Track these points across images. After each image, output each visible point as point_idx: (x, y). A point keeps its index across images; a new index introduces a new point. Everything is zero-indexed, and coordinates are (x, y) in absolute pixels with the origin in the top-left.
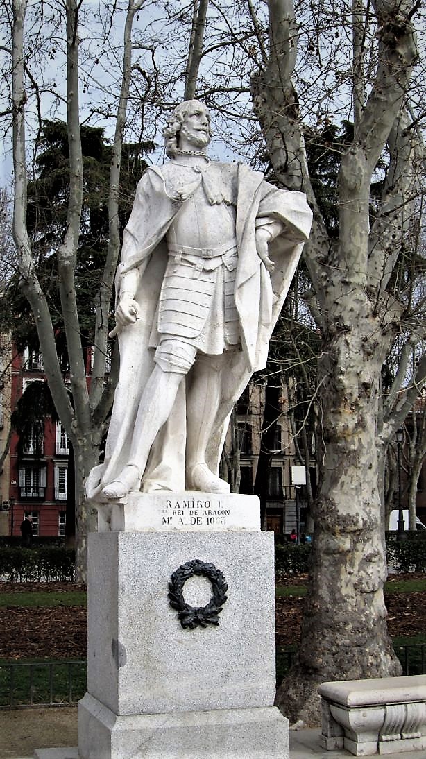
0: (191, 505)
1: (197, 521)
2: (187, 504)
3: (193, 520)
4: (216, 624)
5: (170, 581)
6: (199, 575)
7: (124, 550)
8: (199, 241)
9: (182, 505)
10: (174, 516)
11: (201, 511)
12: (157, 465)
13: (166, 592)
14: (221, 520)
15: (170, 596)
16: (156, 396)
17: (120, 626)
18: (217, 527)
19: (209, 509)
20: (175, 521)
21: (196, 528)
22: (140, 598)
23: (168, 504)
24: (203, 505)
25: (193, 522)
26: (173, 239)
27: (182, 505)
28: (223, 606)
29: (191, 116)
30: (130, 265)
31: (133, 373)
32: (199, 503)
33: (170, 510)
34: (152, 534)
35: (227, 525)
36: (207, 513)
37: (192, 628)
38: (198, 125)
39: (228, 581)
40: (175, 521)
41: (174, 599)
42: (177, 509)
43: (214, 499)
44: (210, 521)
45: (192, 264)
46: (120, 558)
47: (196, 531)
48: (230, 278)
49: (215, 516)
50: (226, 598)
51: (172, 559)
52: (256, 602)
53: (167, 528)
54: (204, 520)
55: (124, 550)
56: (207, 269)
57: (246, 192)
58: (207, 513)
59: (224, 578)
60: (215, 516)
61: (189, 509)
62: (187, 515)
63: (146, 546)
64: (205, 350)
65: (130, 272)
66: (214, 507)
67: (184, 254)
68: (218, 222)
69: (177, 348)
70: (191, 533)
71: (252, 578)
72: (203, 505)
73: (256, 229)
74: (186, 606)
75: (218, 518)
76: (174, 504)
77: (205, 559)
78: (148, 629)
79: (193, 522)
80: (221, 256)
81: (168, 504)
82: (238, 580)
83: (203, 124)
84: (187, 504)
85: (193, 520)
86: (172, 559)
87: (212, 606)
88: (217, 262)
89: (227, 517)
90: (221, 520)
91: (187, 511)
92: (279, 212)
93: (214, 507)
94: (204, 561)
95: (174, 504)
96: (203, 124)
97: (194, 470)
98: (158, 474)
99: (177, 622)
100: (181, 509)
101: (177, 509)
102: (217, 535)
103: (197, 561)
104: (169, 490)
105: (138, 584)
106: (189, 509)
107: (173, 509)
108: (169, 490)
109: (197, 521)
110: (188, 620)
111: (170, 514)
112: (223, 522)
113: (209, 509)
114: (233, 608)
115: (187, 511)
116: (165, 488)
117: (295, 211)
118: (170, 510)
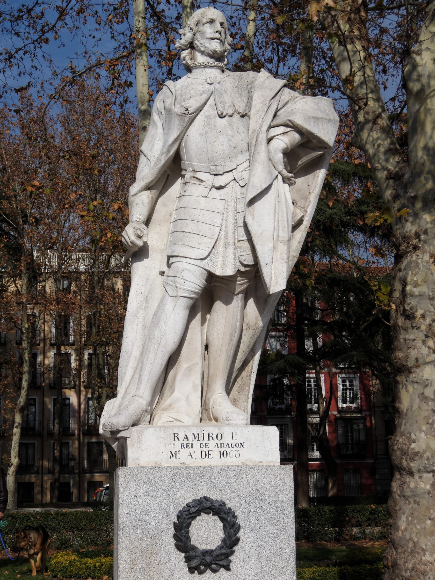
0: (201, 438)
1: (208, 455)
2: (196, 437)
3: (204, 453)
4: (228, 568)
5: (176, 520)
6: (208, 513)
7: (125, 486)
8: (208, 156)
9: (191, 437)
10: (182, 450)
11: (212, 444)
12: (171, 395)
13: (172, 531)
14: (235, 453)
15: (175, 536)
16: (162, 322)
17: (120, 570)
18: (229, 461)
19: (221, 441)
20: (184, 455)
21: (206, 462)
22: (142, 539)
23: (176, 437)
24: (214, 436)
25: (204, 456)
26: (184, 155)
27: (191, 437)
28: (235, 548)
29: (204, 24)
30: (140, 187)
31: (142, 299)
32: (211, 435)
33: (178, 444)
34: (158, 468)
35: (242, 459)
36: (219, 445)
37: (201, 572)
38: (211, 33)
39: (241, 520)
40: (184, 455)
41: (181, 541)
42: (185, 442)
43: (227, 431)
44: (222, 454)
45: (202, 181)
46: (120, 496)
47: (206, 465)
48: (242, 193)
49: (228, 450)
50: (238, 540)
51: (178, 496)
52: (274, 544)
53: (174, 462)
54: (215, 454)
55: (125, 486)
56: (217, 185)
57: (260, 101)
58: (219, 445)
59: (235, 517)
60: (228, 450)
61: (199, 442)
62: (197, 449)
63: (149, 482)
64: (218, 273)
65: (140, 194)
66: (227, 440)
67: (194, 171)
68: (227, 135)
69: (182, 270)
70: (198, 468)
71: (268, 516)
72: (214, 436)
73: (269, 140)
74: (194, 548)
75: (232, 451)
76: (181, 436)
77: (215, 496)
78: (151, 573)
79: (204, 456)
80: (232, 171)
81: (176, 437)
82: (253, 519)
83: (217, 32)
84: (196, 437)
85: (204, 453)
86: (178, 496)
87: (223, 547)
88: (228, 177)
89: (241, 449)
90: (235, 453)
91: (196, 444)
92: (294, 120)
93: (227, 440)
94: (214, 498)
95: (181, 436)
96: (217, 32)
97: (212, 401)
98: (170, 405)
99: (184, 566)
100: (190, 442)
101: (185, 442)
102: (229, 468)
103: (205, 498)
104: (180, 421)
105: (140, 523)
106: (199, 442)
107: (181, 442)
108: (180, 421)
109: (208, 455)
110: (194, 563)
111: (178, 448)
112: (238, 455)
113: (221, 441)
114: (247, 550)
115: (196, 444)
116: (176, 420)
117: (313, 117)
118: (178, 444)
